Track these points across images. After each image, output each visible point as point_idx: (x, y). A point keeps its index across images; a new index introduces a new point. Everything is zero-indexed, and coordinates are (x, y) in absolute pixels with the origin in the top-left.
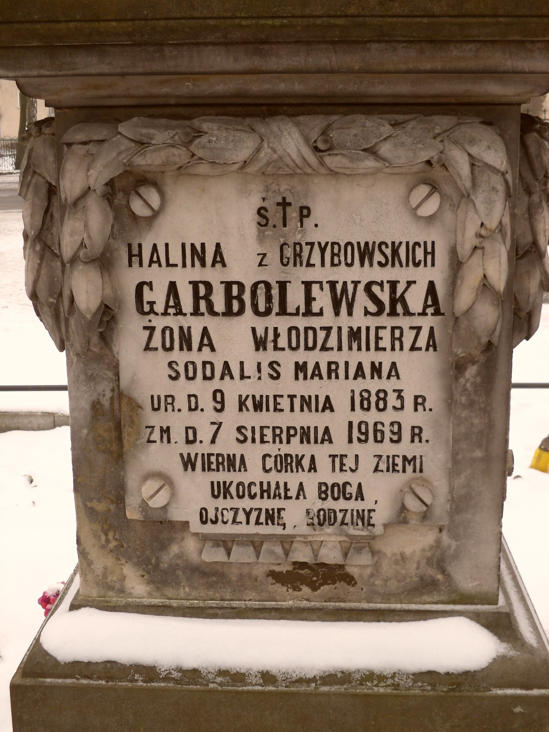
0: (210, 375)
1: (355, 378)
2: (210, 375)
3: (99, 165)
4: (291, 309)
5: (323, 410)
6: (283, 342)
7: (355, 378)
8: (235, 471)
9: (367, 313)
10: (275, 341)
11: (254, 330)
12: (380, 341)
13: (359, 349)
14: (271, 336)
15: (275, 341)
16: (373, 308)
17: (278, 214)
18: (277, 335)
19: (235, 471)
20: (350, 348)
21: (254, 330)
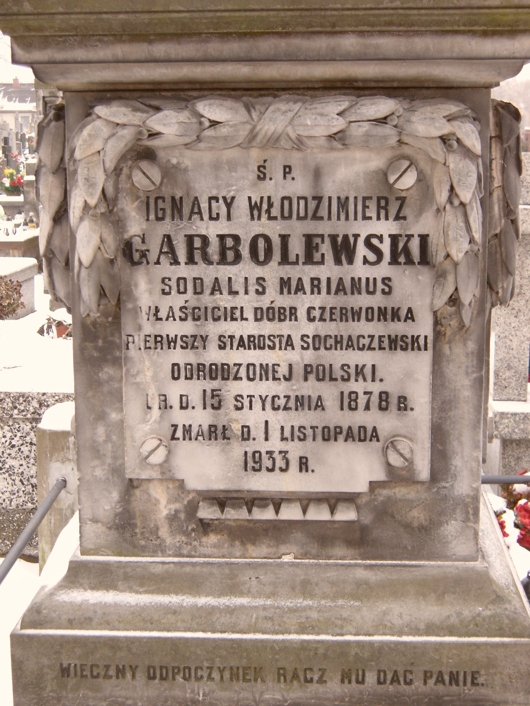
0: (190, 377)
1: (336, 293)
2: (190, 377)
3: (119, 415)
4: (292, 258)
5: (296, 293)
6: (276, 212)
7: (336, 293)
8: (190, 439)
9: (366, 261)
10: (268, 211)
11: (250, 198)
12: (367, 210)
13: (347, 218)
14: (265, 206)
15: (268, 211)
16: (372, 257)
17: (306, 270)
18: (270, 205)
19: (190, 439)
20: (339, 218)
21: (250, 198)
